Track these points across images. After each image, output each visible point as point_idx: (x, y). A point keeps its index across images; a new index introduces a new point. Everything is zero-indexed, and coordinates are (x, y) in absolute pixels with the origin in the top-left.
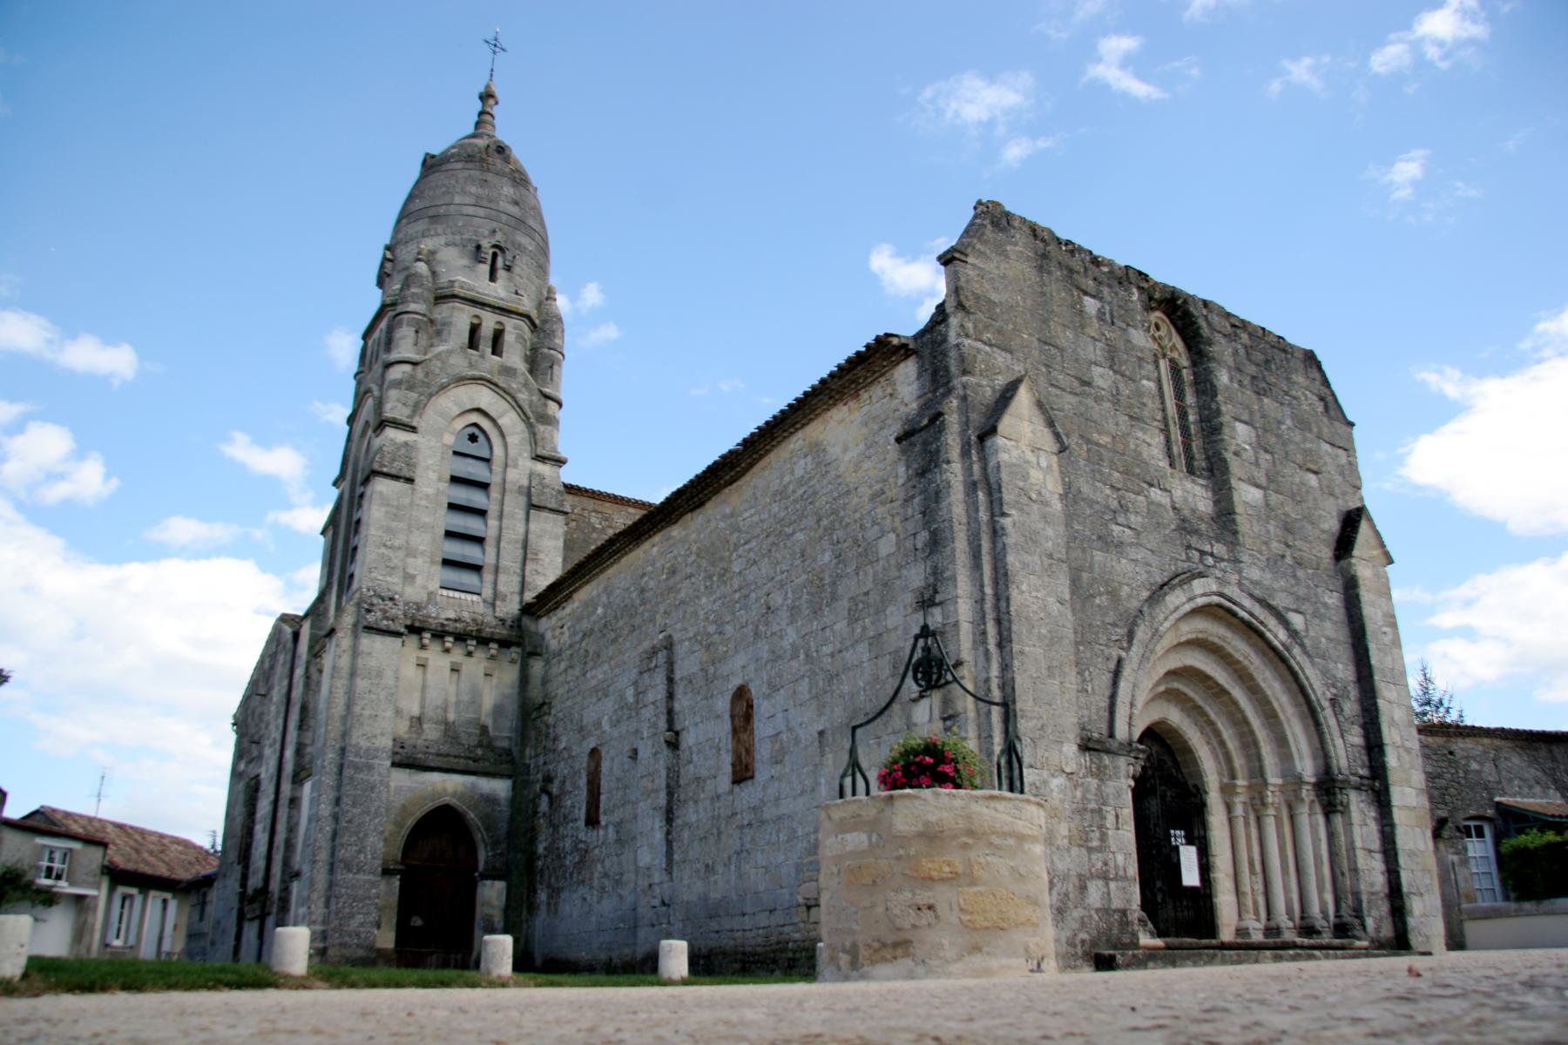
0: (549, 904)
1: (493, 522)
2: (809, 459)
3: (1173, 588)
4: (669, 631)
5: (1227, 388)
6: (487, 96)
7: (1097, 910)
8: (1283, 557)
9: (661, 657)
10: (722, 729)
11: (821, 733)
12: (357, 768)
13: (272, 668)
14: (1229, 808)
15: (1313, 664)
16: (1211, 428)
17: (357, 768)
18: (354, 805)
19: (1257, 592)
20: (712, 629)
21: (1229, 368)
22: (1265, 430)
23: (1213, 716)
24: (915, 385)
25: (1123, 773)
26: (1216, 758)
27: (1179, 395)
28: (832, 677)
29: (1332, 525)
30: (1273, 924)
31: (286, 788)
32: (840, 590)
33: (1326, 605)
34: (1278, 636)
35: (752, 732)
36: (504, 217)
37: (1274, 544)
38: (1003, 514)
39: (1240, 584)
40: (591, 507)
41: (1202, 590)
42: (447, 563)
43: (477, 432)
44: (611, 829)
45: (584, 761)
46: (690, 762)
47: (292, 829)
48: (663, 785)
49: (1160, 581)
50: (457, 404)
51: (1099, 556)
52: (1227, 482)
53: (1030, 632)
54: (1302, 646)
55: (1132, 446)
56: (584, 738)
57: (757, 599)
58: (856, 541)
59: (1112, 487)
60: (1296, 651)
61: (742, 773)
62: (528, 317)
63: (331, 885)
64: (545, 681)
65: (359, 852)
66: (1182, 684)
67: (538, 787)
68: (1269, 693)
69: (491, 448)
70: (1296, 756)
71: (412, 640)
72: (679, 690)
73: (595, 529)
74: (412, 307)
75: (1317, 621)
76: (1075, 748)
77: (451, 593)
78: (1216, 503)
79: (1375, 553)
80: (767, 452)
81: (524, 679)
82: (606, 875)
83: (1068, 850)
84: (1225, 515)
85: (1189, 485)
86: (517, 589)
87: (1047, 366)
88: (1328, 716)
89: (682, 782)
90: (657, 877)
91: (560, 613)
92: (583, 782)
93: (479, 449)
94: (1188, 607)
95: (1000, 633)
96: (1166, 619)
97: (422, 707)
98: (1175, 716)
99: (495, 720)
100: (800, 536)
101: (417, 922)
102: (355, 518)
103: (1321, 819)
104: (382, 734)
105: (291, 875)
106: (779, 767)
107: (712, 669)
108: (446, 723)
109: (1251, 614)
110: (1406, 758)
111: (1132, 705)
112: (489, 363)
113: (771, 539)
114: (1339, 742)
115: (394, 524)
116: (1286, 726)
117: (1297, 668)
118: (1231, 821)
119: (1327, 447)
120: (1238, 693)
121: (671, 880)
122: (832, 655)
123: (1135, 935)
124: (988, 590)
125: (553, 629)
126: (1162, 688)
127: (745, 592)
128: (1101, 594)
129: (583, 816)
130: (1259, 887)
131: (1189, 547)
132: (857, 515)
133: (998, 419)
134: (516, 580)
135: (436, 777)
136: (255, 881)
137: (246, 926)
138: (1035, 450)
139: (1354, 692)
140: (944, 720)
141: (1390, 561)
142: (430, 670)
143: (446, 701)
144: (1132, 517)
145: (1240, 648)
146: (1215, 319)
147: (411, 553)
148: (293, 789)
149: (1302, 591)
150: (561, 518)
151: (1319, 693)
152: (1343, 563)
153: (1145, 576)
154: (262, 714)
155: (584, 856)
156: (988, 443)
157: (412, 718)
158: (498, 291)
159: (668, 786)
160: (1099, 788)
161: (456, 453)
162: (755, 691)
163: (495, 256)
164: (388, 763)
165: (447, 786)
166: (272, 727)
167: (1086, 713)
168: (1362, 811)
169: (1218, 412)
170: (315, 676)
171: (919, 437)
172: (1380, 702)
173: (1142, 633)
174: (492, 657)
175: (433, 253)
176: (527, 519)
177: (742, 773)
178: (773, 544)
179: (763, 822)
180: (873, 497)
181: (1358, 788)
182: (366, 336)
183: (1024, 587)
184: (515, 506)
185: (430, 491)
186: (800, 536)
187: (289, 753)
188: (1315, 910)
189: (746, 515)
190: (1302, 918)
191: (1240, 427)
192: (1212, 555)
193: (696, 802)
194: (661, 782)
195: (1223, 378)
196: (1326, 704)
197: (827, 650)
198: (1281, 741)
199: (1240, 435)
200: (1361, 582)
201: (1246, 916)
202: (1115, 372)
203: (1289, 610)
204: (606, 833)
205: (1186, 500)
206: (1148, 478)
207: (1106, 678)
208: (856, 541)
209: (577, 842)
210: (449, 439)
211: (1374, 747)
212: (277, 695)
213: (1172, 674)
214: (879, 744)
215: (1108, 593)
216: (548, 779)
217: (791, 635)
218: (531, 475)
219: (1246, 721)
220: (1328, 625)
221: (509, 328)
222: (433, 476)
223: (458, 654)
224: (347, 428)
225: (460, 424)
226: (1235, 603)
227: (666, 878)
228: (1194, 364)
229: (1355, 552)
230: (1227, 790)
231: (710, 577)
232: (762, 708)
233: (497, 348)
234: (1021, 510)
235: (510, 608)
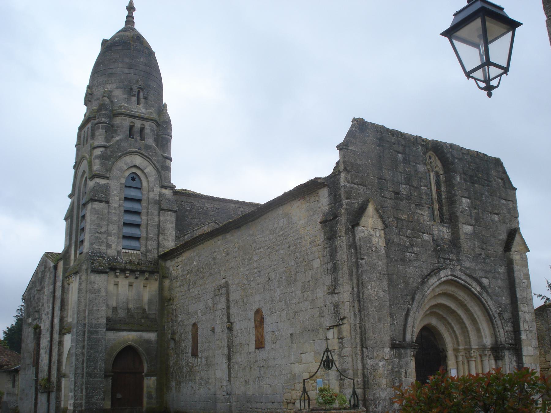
0: (176, 388)
1: (144, 218)
2: (285, 219)
3: (432, 276)
4: (227, 279)
6: (131, 8)
8: (481, 254)
9: (224, 290)
10: (251, 325)
11: (291, 335)
13: (43, 278)
14: (456, 357)
15: (492, 299)
20: (246, 282)
21: (460, 173)
23: (450, 321)
24: (327, 199)
25: (409, 355)
26: (452, 337)
27: (438, 186)
28: (296, 313)
29: (503, 236)
31: (56, 336)
33: (499, 273)
34: (476, 289)
36: (142, 73)
37: (477, 250)
38: (362, 259)
39: (461, 270)
40: (185, 200)
41: (444, 275)
42: (125, 237)
43: (135, 176)
44: (203, 359)
46: (238, 337)
47: (60, 354)
48: (226, 345)
49: (426, 273)
50: (126, 164)
51: (401, 267)
52: (457, 225)
54: (487, 292)
55: (416, 218)
56: (190, 318)
58: (304, 259)
59: (407, 237)
60: (485, 295)
61: (260, 345)
62: (156, 121)
64: (170, 289)
65: (95, 369)
67: (169, 336)
68: (473, 312)
69: (141, 183)
70: (484, 336)
71: (112, 274)
72: (232, 305)
73: (187, 210)
75: (494, 280)
76: (389, 349)
77: (127, 251)
78: (453, 234)
79: (522, 248)
81: (161, 288)
82: (202, 379)
83: (386, 389)
84: (455, 242)
85: (441, 228)
86: (156, 247)
87: (380, 189)
89: (234, 344)
90: (225, 383)
91: (176, 260)
92: (190, 337)
94: (438, 283)
95: (360, 306)
96: (428, 289)
97: (117, 303)
98: (434, 322)
99: (149, 307)
100: (281, 252)
101: (119, 396)
102: (81, 214)
104: (102, 317)
105: (61, 375)
107: (246, 299)
108: (128, 310)
109: (465, 282)
110: (530, 335)
111: (413, 327)
113: (269, 250)
114: (501, 331)
115: (101, 222)
116: (480, 325)
117: (484, 302)
118: (457, 362)
119: (504, 202)
120: (460, 312)
121: (231, 384)
124: (355, 289)
125: (173, 267)
127: (259, 269)
128: (401, 283)
131: (439, 257)
132: (305, 248)
133: (360, 219)
134: (155, 243)
135: (125, 334)
136: (43, 375)
137: (39, 395)
138: (374, 229)
139: (509, 308)
140: (339, 339)
141: (528, 251)
142: (120, 285)
143: (128, 299)
144: (415, 249)
145: (461, 295)
146: (455, 153)
147: (108, 234)
149: (488, 268)
150: (174, 214)
152: (507, 253)
153: (420, 272)
154: (39, 299)
155: (192, 370)
156: (356, 228)
157: (113, 308)
158: (141, 110)
159: (228, 345)
160: (399, 362)
161: (126, 186)
162: (265, 311)
163: (139, 92)
164: (105, 330)
165: (129, 337)
166: (46, 306)
167: (394, 333)
168: (510, 358)
169: (455, 195)
170: (66, 286)
171: (329, 222)
172: (520, 313)
173: (417, 297)
174: (147, 279)
175: (111, 92)
176: (159, 215)
177: (260, 345)
178: (270, 252)
180: (311, 242)
181: (509, 349)
185: (116, 206)
186: (281, 252)
187: (56, 321)
191: (464, 200)
192: (449, 259)
193: (240, 354)
194: (225, 343)
196: (496, 315)
197: (293, 301)
198: (478, 330)
202: (410, 186)
203: (481, 277)
204: (200, 361)
205: (439, 234)
206: (422, 231)
207: (402, 318)
208: (304, 259)
209: (188, 363)
210: (123, 181)
211: (516, 331)
212: (47, 290)
214: (314, 343)
215: (404, 282)
216: (173, 333)
217: (279, 292)
219: (463, 323)
220: (499, 281)
221: (147, 127)
222: (117, 199)
223: (132, 279)
224: (74, 171)
225: (127, 174)
226: (458, 278)
227: (228, 384)
228: (445, 173)
229: (513, 249)
230: (456, 350)
231: (244, 260)
232: (268, 320)
234: (368, 256)
235: (154, 255)
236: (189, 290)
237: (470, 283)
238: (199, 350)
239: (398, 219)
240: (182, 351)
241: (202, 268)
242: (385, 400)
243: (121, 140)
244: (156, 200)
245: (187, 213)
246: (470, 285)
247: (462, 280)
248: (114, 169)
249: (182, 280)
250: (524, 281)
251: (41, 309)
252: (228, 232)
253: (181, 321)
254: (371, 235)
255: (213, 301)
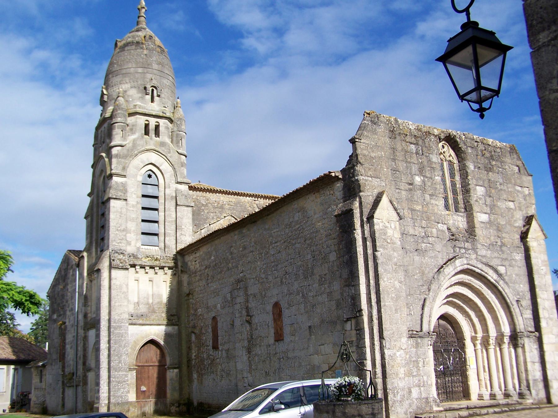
1: (162, 214)
5: (473, 171)
7: (416, 399)
10: (269, 318)
11: (310, 327)
12: (115, 328)
15: (509, 286)
16: (466, 190)
17: (115, 328)
18: (115, 343)
19: (484, 260)
22: (490, 185)
24: (342, 192)
27: (452, 176)
28: (313, 306)
30: (493, 392)
32: (315, 271)
33: (515, 260)
34: (492, 276)
35: (282, 322)
39: (476, 258)
40: (200, 195)
41: (459, 264)
45: (210, 321)
46: (256, 329)
52: (472, 214)
53: (388, 297)
54: (504, 280)
57: (281, 268)
60: (501, 282)
61: (279, 337)
63: (109, 377)
66: (456, 299)
68: (490, 300)
73: (203, 204)
74: (119, 119)
75: (511, 268)
76: (406, 339)
77: (146, 247)
78: (468, 222)
80: (282, 207)
82: (223, 370)
84: (471, 231)
88: (515, 309)
92: (210, 330)
93: (153, 180)
97: (138, 298)
100: (297, 245)
101: (144, 388)
103: (513, 350)
104: (124, 313)
106: (293, 337)
107: (264, 293)
108: (148, 304)
110: (551, 323)
112: (152, 141)
113: (286, 244)
114: (520, 318)
118: (475, 350)
119: (519, 188)
122: (313, 297)
123: (431, 406)
126: (445, 301)
127: (276, 263)
129: (211, 345)
130: (487, 377)
132: (321, 242)
148: (85, 333)
149: (505, 256)
150: (190, 209)
151: (511, 299)
158: (155, 108)
163: (153, 90)
164: (128, 324)
173: (433, 287)
177: (279, 337)
178: (287, 246)
179: (288, 358)
181: (528, 337)
182: (97, 128)
183: (385, 279)
184: (171, 205)
185: (135, 203)
186: (297, 245)
188: (510, 386)
189: (275, 231)
190: (505, 390)
192: (465, 248)
193: (260, 346)
195: (471, 167)
196: (515, 303)
199: (478, 192)
200: (531, 249)
201: (481, 389)
204: (221, 354)
205: (454, 224)
206: (437, 221)
209: (209, 355)
210: (140, 179)
213: (448, 297)
217: (296, 285)
218: (176, 190)
219: (480, 311)
230: (474, 339)
232: (286, 313)
233: (157, 133)
236: (208, 284)
237: (486, 271)
238: (219, 343)
239: (413, 210)
240: (203, 344)
241: (220, 262)
242: (403, 389)
243: (138, 138)
244: (172, 197)
245: (203, 208)
246: (486, 273)
247: (478, 268)
248: (131, 166)
249: (201, 274)
250: (542, 268)
251: (65, 305)
252: (245, 227)
253: (200, 315)
254: (387, 227)
255: (231, 295)
